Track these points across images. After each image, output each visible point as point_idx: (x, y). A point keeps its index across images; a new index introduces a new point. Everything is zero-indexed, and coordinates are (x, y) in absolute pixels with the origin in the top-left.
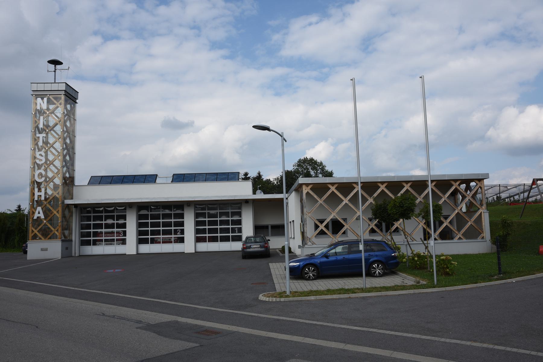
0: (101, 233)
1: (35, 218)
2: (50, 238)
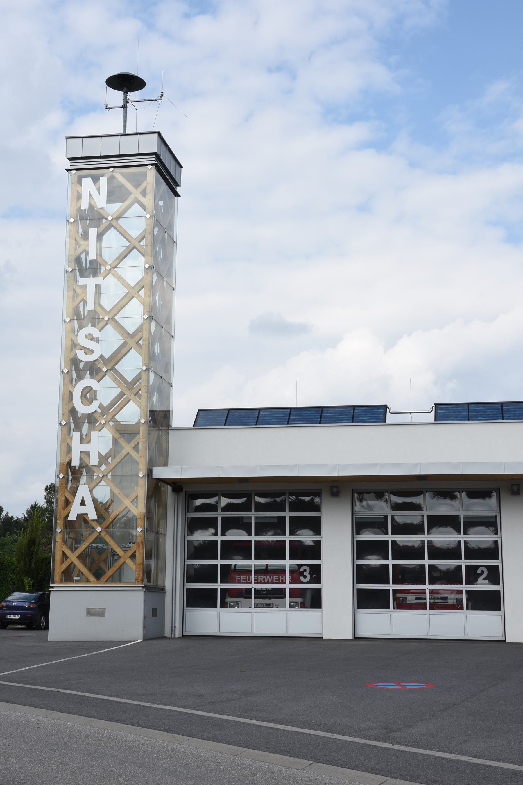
0: (247, 571)
1: (72, 517)
2: (111, 579)
